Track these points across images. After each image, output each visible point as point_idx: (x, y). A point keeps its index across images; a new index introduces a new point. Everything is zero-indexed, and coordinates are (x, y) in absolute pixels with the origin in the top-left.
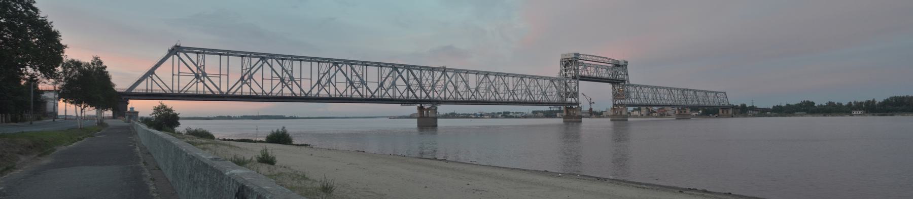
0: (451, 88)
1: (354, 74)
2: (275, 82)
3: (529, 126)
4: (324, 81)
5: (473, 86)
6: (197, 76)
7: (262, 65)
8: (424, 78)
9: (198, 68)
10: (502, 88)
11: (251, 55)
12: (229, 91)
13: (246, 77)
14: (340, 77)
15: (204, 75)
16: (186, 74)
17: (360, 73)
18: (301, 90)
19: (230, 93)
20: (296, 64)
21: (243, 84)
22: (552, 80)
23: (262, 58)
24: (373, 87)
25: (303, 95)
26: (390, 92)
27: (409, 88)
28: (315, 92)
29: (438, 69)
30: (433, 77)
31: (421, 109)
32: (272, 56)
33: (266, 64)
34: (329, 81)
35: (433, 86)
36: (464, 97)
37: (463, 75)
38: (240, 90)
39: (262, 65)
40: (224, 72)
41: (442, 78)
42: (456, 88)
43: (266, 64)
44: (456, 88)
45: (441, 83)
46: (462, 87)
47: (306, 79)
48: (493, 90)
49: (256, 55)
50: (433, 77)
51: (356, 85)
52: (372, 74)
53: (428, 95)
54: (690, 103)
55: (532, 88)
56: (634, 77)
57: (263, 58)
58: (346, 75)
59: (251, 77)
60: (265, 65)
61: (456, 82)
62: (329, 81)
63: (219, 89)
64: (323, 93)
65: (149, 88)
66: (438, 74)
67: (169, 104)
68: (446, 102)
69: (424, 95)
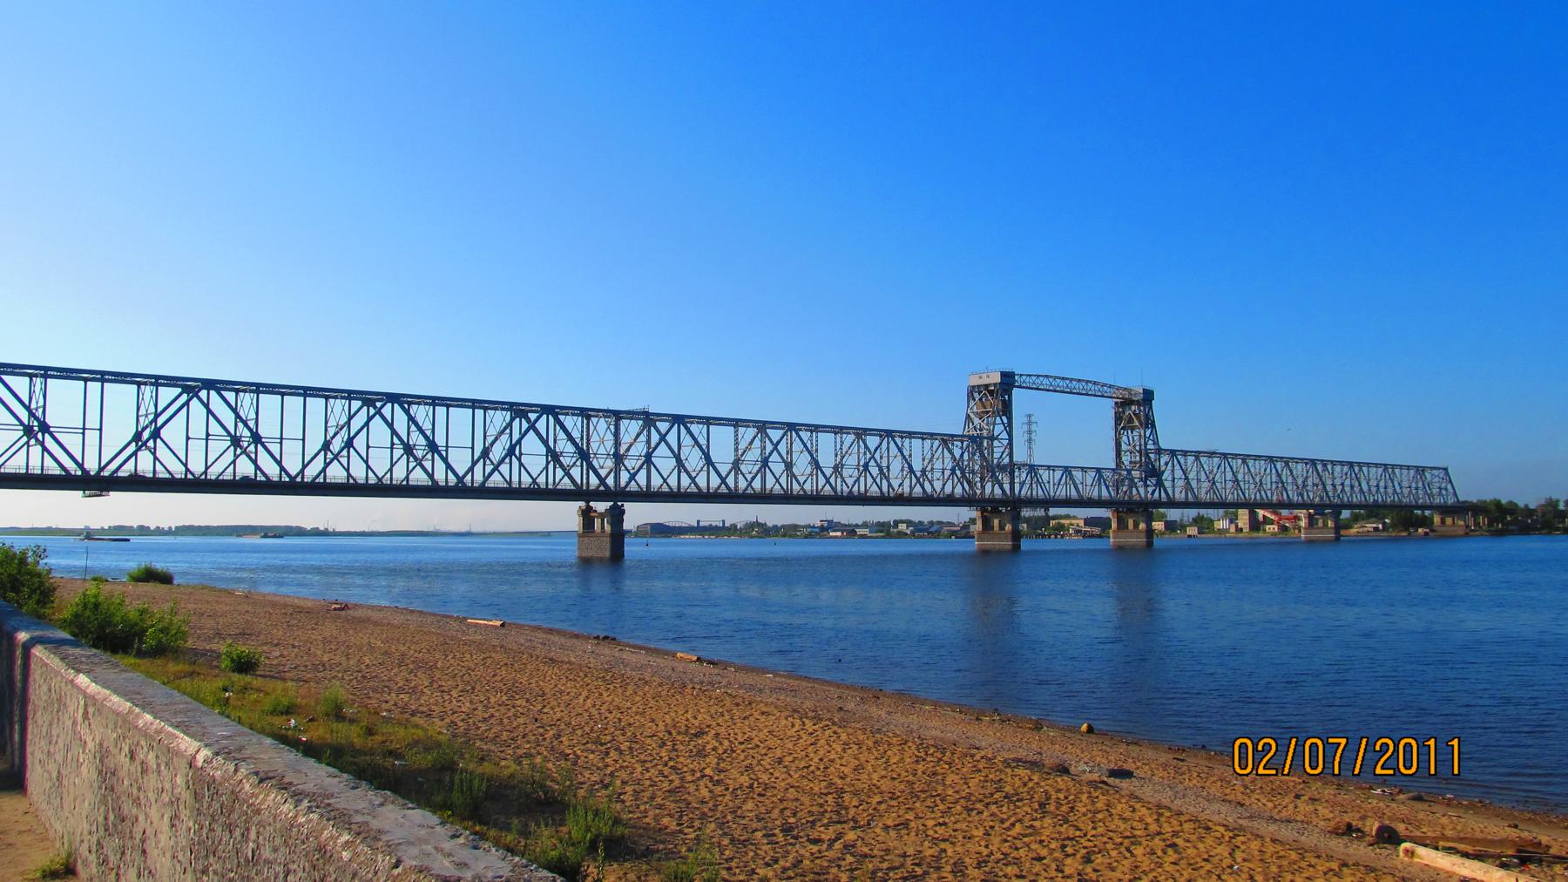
0: (778, 467)
1: (561, 435)
2: (217, 447)
3: (778, 560)
4: (336, 445)
5: (827, 461)
6: (28, 431)
7: (187, 403)
8: (594, 438)
9: (32, 414)
10: (896, 466)
11: (158, 381)
12: (101, 469)
13: (146, 435)
14: (532, 444)
15: (45, 428)
16: (218, 438)
17: (427, 426)
18: (282, 469)
19: (106, 473)
20: (269, 402)
21: (139, 449)
22: (946, 440)
23: (186, 389)
24: (461, 461)
25: (372, 480)
26: (641, 478)
27: (680, 464)
28: (399, 473)
29: (632, 415)
30: (616, 434)
31: (587, 516)
32: (210, 384)
33: (195, 401)
34: (349, 444)
35: (619, 458)
36: (807, 487)
37: (805, 435)
38: (130, 466)
39: (187, 403)
40: (93, 422)
41: (757, 443)
42: (789, 466)
43: (195, 401)
44: (789, 466)
45: (754, 454)
46: (802, 465)
47: (296, 438)
48: (875, 471)
49: (171, 381)
50: (616, 434)
51: (419, 454)
52: (722, 443)
53: (602, 481)
54: (1438, 500)
55: (1240, 477)
56: (1172, 431)
57: (191, 387)
58: (391, 425)
59: (156, 434)
60: (195, 403)
61: (790, 452)
62: (349, 444)
63: (81, 466)
64: (336, 473)
65: (515, 479)
66: (630, 428)
67: (1203, 512)
68: (647, 496)
69: (715, 482)
